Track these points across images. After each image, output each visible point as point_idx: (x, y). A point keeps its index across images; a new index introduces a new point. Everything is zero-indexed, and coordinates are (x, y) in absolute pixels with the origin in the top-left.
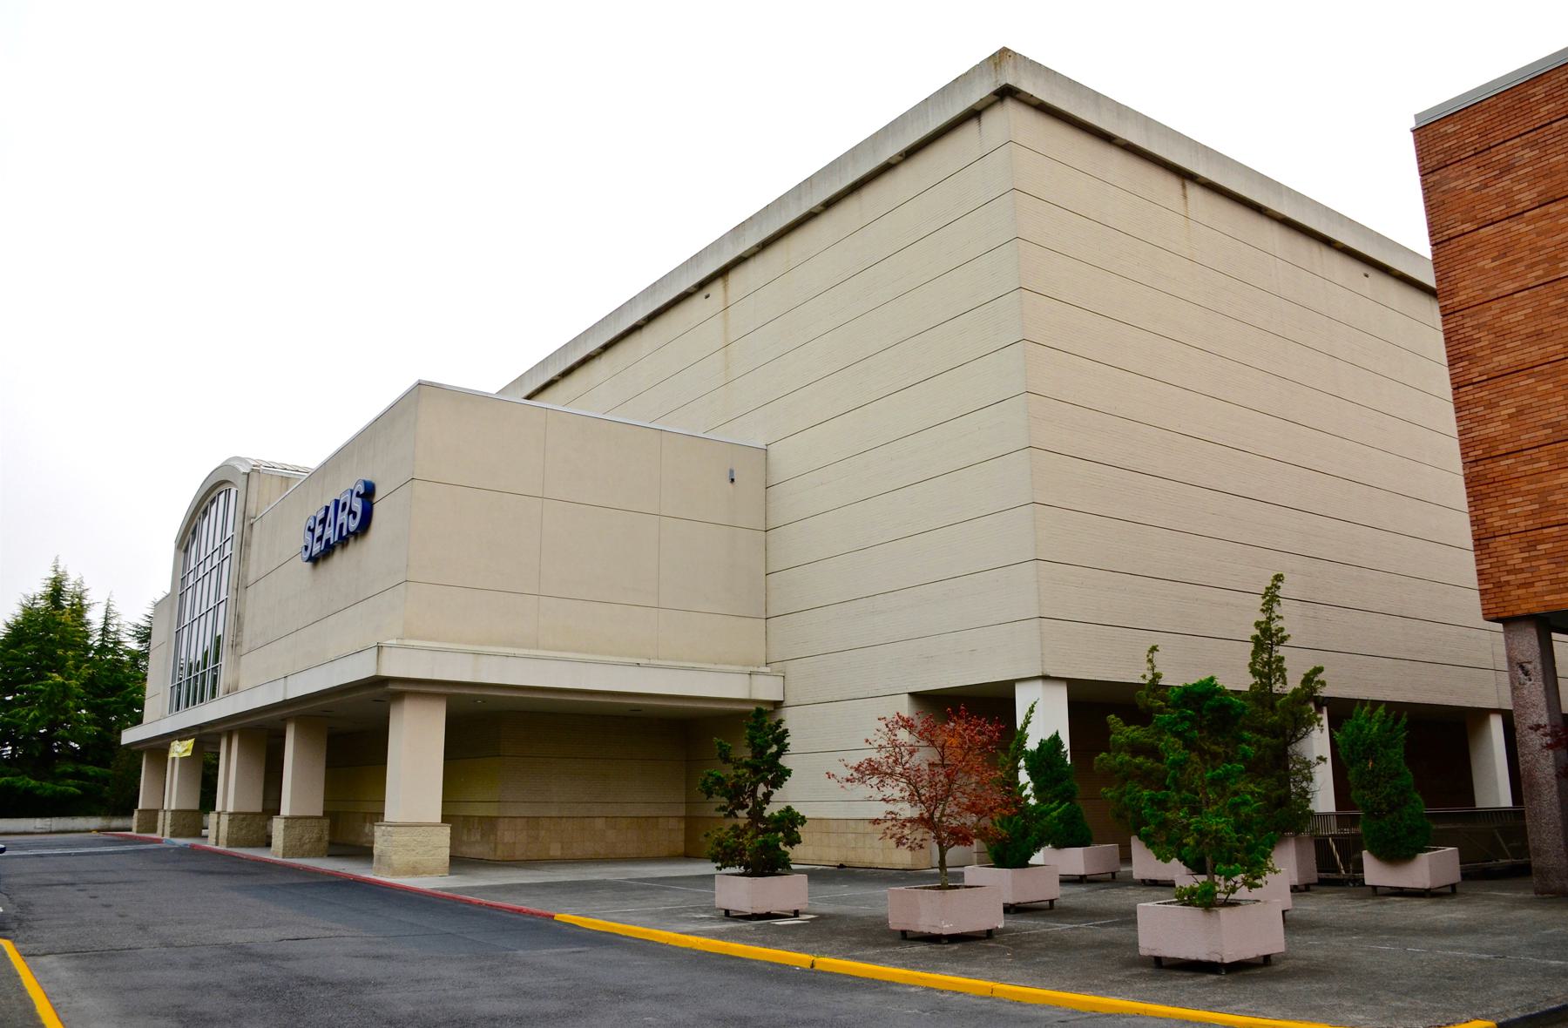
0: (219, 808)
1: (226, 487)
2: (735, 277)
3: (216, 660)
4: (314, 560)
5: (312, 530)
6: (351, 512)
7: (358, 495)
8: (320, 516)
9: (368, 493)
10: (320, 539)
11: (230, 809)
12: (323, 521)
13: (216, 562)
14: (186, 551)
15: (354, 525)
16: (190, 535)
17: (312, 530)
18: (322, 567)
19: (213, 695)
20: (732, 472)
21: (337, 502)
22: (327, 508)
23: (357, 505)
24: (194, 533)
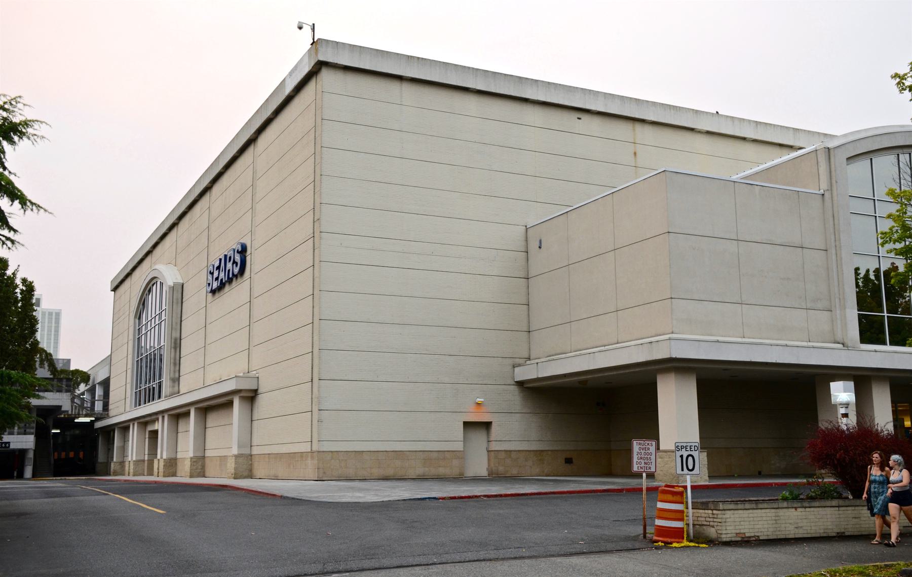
0: (159, 456)
1: (154, 281)
2: (586, 118)
3: (160, 378)
4: (213, 292)
5: (212, 273)
6: (234, 262)
7: (238, 252)
8: (217, 264)
9: (243, 250)
10: (217, 279)
11: (165, 457)
12: (218, 268)
13: (157, 322)
14: (139, 318)
15: (236, 270)
16: (141, 306)
17: (212, 273)
18: (217, 295)
19: (159, 397)
20: (540, 241)
21: (226, 256)
22: (220, 260)
23: (238, 258)
24: (144, 304)
